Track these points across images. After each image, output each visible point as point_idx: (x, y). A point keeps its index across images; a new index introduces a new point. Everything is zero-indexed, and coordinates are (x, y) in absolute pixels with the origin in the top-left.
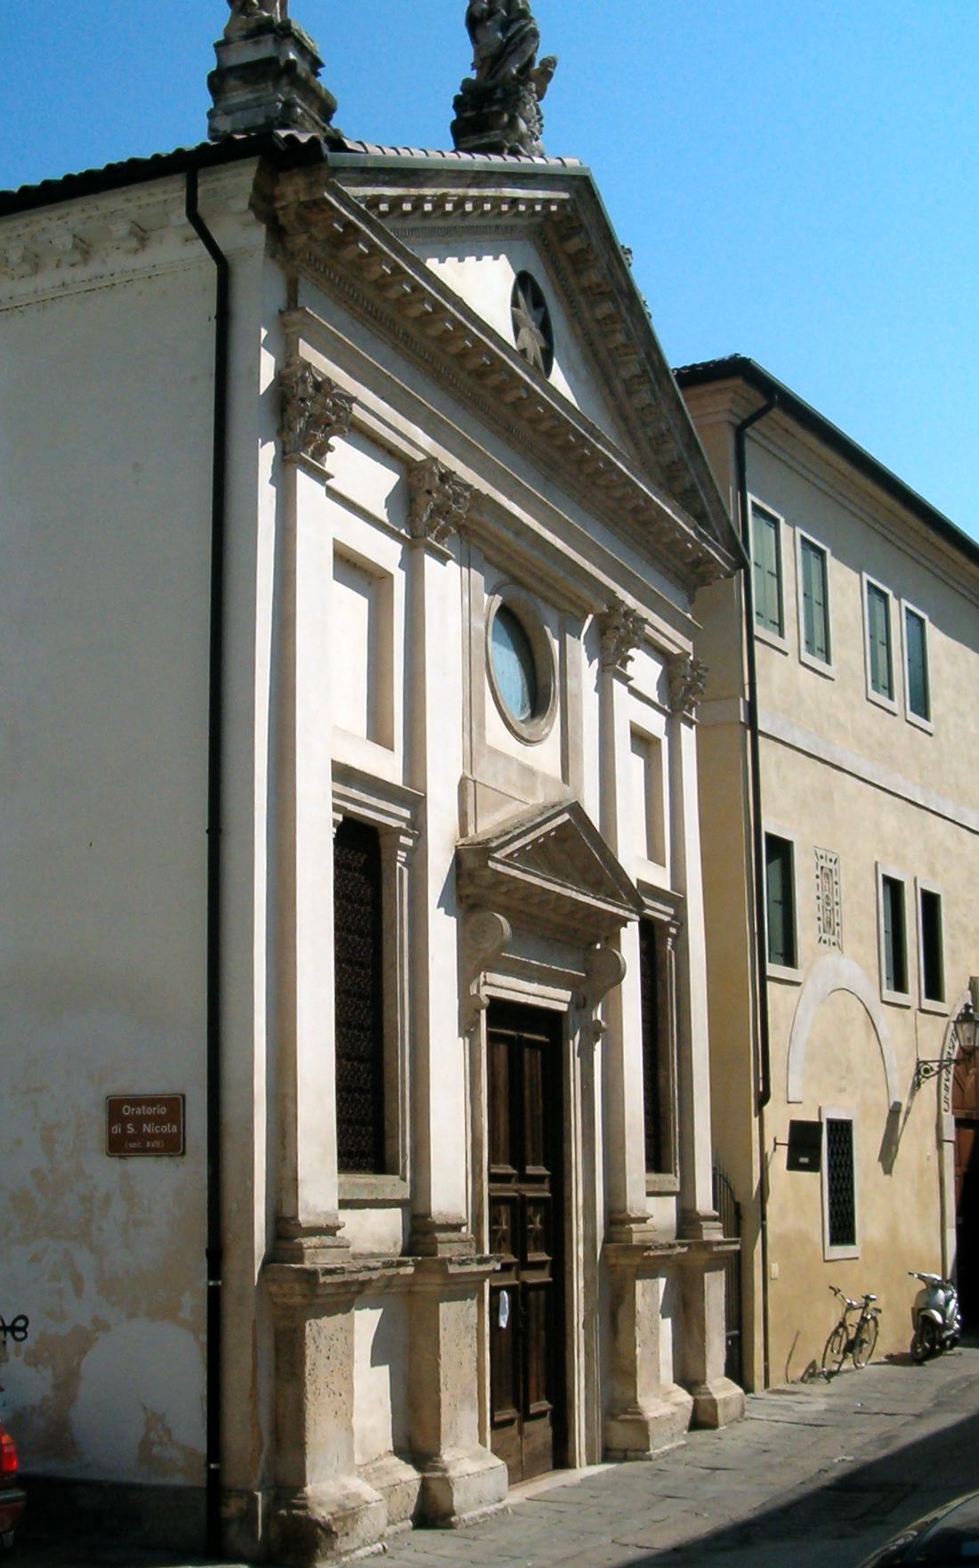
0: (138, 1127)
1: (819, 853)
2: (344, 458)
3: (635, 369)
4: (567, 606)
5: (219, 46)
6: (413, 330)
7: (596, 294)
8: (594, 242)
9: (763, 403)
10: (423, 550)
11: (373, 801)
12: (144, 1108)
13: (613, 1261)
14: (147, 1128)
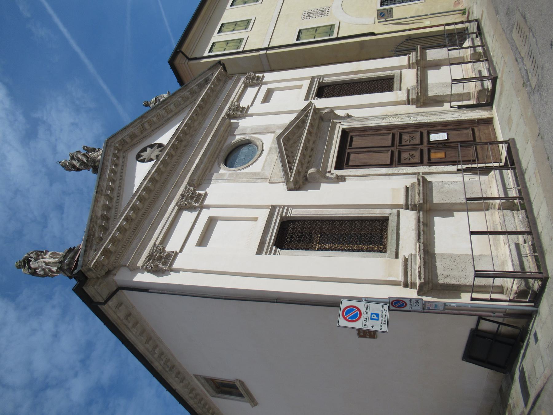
1: (303, 18)
2: (244, 103)
3: (163, 112)
4: (226, 135)
6: (140, 213)
7: (143, 129)
8: (126, 134)
9: (181, 54)
10: (247, 114)
11: (273, 225)
13: (422, 104)
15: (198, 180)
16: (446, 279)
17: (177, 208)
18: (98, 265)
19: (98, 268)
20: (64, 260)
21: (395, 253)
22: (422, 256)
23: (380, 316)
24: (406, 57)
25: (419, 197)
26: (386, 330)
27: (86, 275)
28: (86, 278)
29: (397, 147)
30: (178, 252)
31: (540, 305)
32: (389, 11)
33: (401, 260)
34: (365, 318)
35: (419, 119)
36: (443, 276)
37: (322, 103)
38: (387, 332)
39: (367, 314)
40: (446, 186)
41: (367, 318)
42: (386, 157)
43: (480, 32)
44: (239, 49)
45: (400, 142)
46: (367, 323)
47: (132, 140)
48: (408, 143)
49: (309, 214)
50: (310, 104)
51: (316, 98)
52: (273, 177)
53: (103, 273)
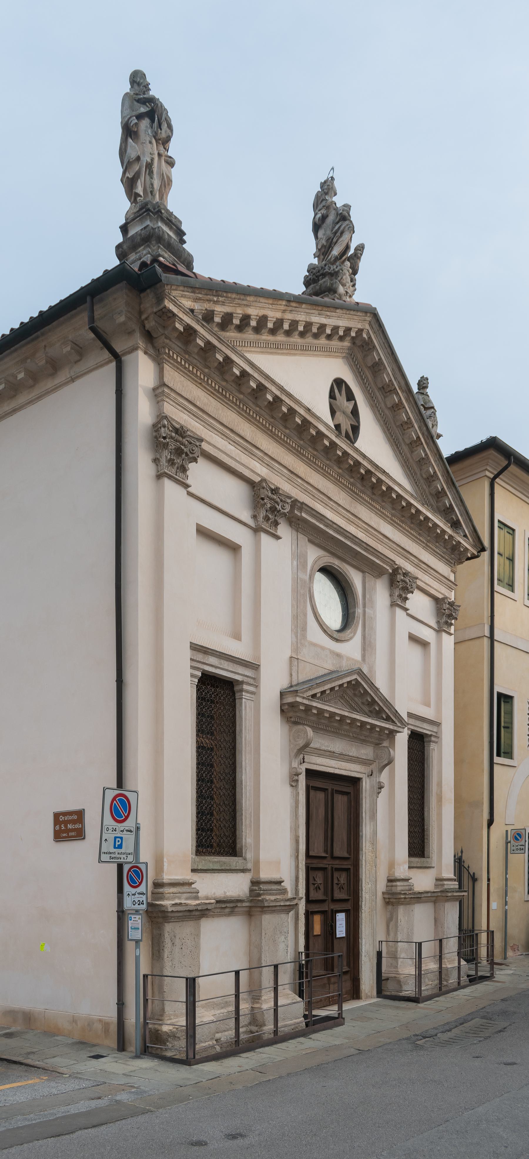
0: (66, 826)
5: (355, 290)
9: (505, 463)
12: (68, 816)
14: (70, 826)
15: (298, 520)
16: (170, 941)
17: (257, 479)
18: (165, 318)
19: (160, 317)
20: (162, 220)
21: (196, 868)
22: (200, 908)
23: (120, 851)
24: (452, 876)
25: (272, 901)
26: (102, 861)
27: (148, 291)
28: (142, 290)
29: (330, 866)
30: (189, 489)
31: (140, 1060)
32: (522, 847)
33: (189, 876)
34: (116, 829)
35: (367, 897)
36: (173, 938)
37: (402, 739)
38: (100, 862)
39: (121, 831)
40: (282, 938)
41: (116, 831)
42: (318, 850)
43: (473, 980)
44: (498, 584)
45: (338, 870)
46: (110, 831)
47: (369, 367)
48: (335, 881)
49: (246, 729)
50: (403, 724)
51: (410, 732)
52: (300, 664)
53: (150, 325)
